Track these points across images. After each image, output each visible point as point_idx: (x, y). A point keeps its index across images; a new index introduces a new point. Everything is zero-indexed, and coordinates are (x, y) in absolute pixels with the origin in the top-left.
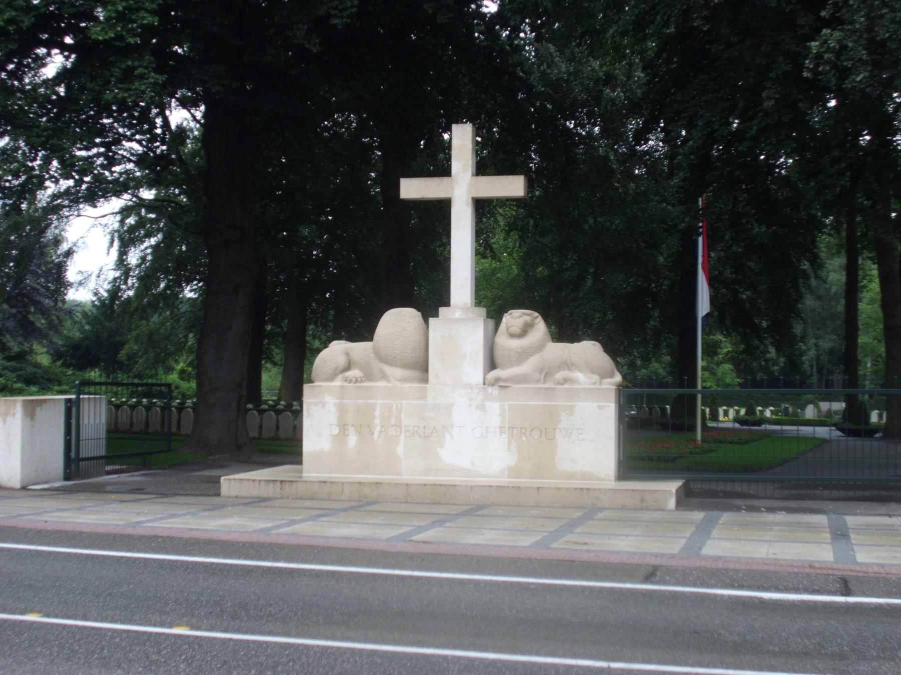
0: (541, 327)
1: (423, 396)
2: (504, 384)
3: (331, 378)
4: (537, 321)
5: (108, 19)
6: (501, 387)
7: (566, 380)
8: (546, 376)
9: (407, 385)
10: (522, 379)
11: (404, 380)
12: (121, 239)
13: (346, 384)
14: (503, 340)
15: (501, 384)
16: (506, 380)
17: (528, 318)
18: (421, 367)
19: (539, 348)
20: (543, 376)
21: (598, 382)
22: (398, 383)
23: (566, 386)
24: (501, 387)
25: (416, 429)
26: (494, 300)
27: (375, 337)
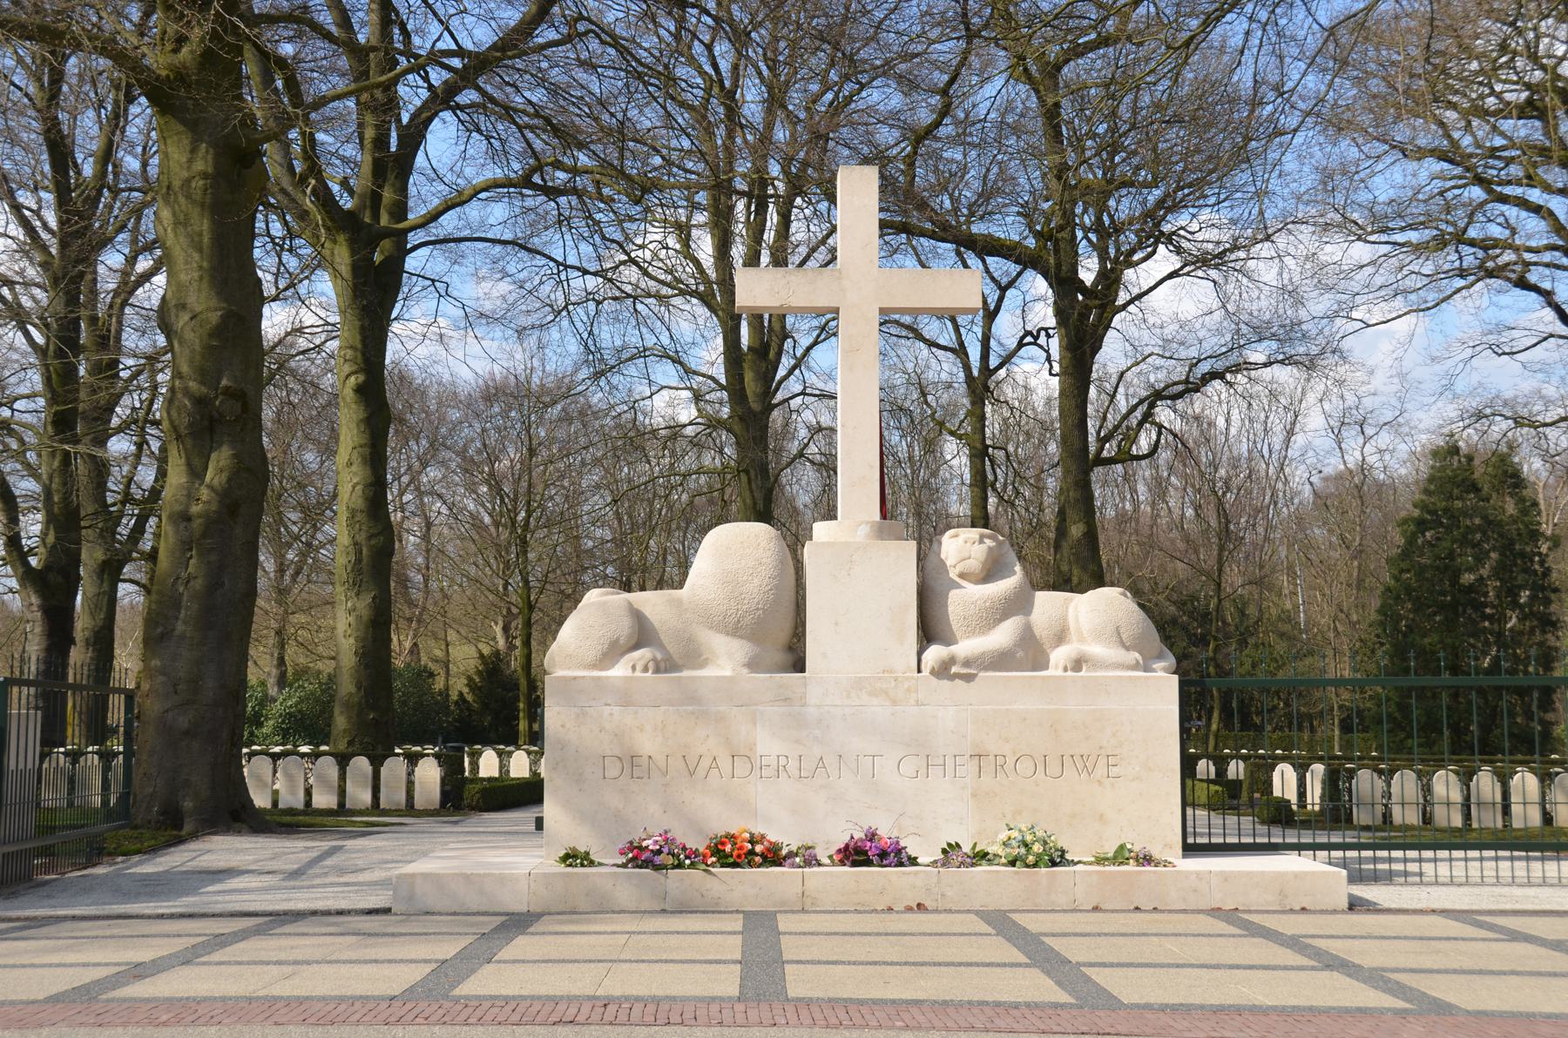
25: (783, 761)
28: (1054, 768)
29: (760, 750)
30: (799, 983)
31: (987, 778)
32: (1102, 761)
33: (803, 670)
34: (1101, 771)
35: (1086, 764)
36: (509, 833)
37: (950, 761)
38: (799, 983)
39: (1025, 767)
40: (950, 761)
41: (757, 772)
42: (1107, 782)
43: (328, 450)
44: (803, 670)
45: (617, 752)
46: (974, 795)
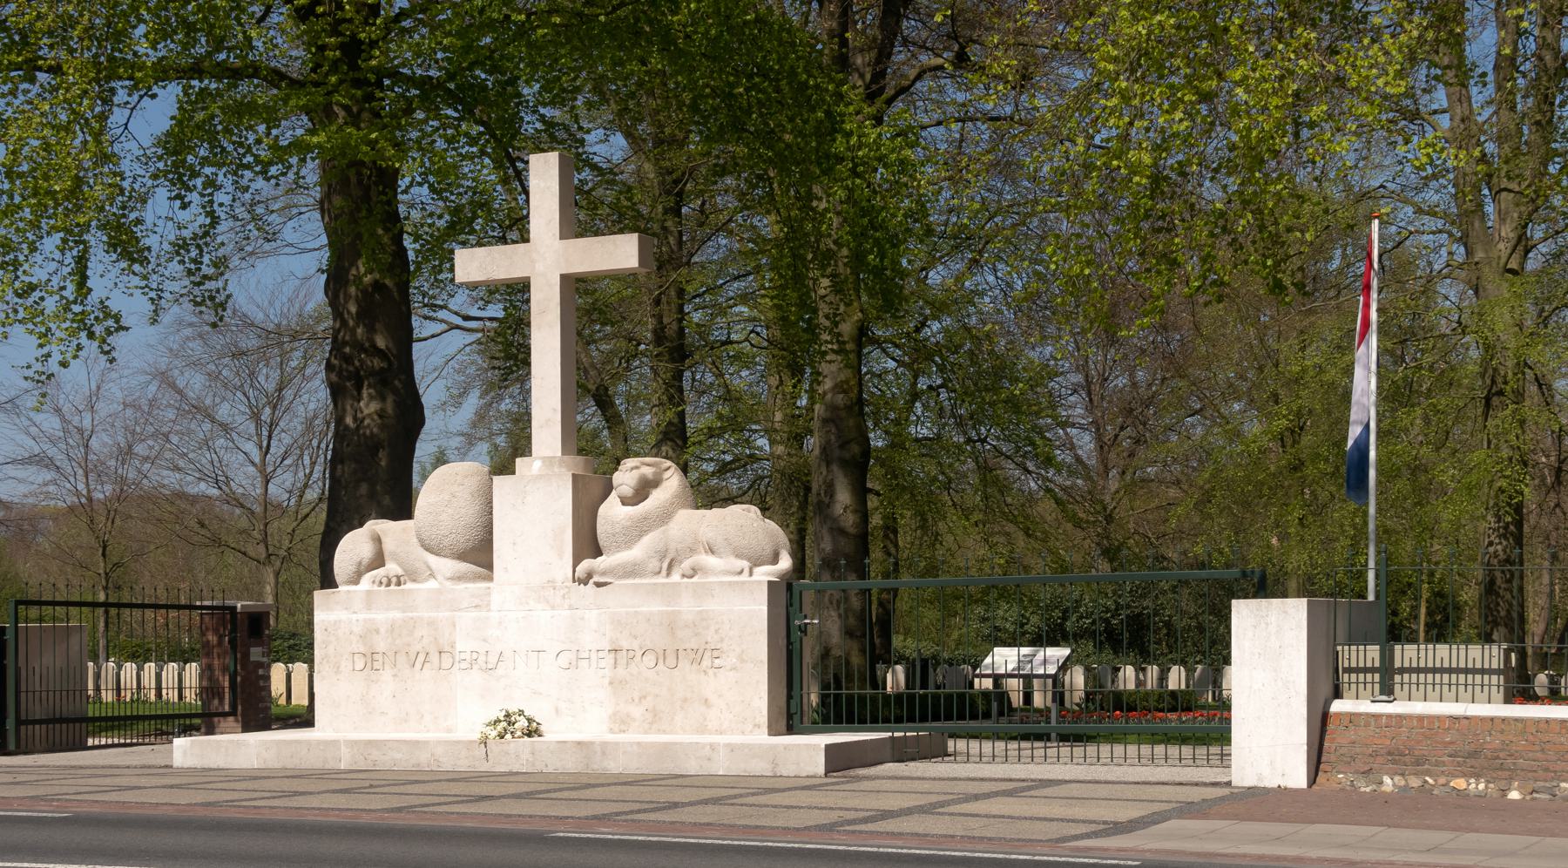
0: (673, 481)
1: (481, 605)
2: (602, 580)
3: (356, 579)
4: (667, 475)
5: (428, 110)
6: (599, 585)
7: (694, 571)
8: (670, 567)
9: (462, 586)
10: (632, 571)
11: (460, 578)
12: (844, 464)
13: (376, 588)
14: (612, 512)
15: (596, 579)
16: (604, 574)
17: (648, 471)
18: (479, 553)
19: (665, 517)
20: (665, 565)
21: (746, 571)
22: (448, 584)
23: (695, 580)
24: (599, 585)
25: (475, 656)
26: (597, 448)
27: (417, 513)
28: (671, 661)
29: (459, 647)
30: (23, 728)
31: (621, 671)
32: (708, 654)
33: (527, 241)
34: (706, 662)
35: (697, 656)
36: (256, 778)
37: (594, 656)
38: (23, 728)
39: (650, 659)
40: (594, 656)
41: (457, 665)
42: (711, 672)
43: (221, 700)
44: (527, 241)
45: (362, 650)
46: (611, 683)
